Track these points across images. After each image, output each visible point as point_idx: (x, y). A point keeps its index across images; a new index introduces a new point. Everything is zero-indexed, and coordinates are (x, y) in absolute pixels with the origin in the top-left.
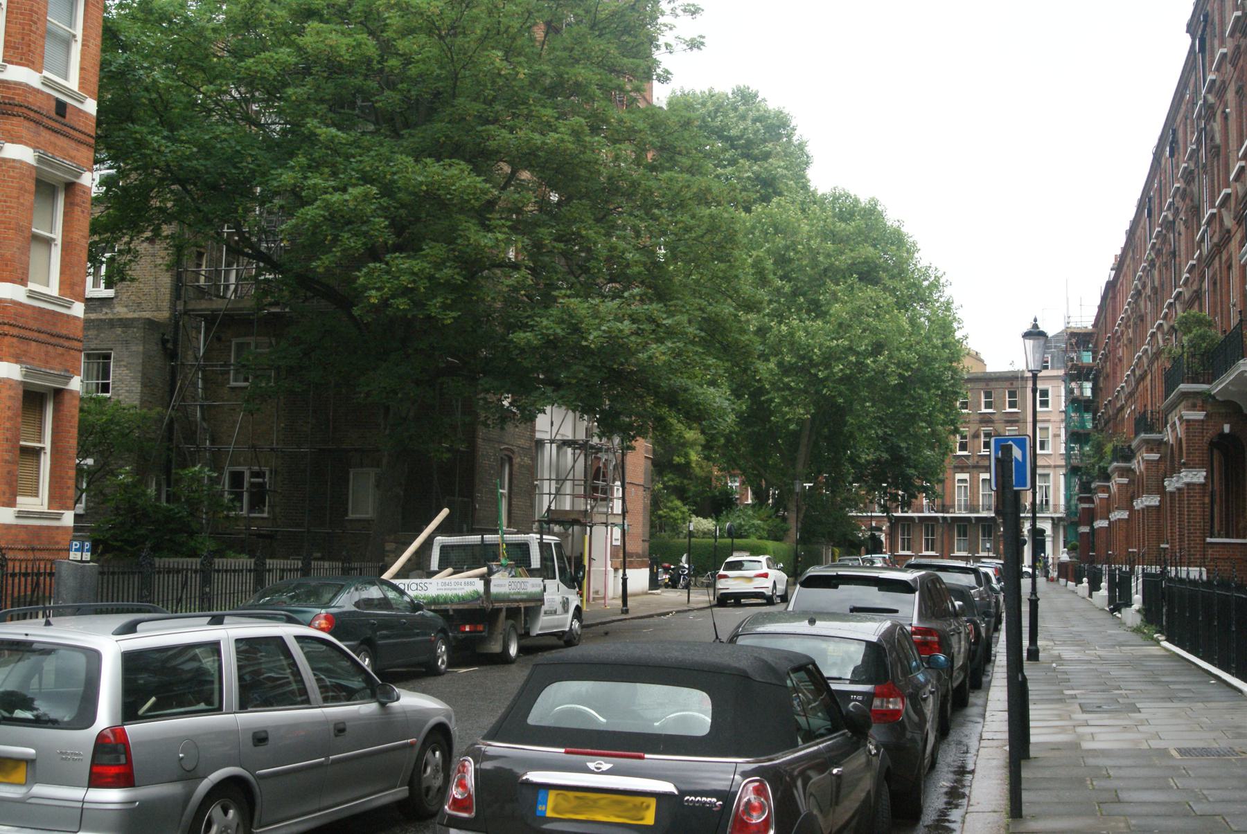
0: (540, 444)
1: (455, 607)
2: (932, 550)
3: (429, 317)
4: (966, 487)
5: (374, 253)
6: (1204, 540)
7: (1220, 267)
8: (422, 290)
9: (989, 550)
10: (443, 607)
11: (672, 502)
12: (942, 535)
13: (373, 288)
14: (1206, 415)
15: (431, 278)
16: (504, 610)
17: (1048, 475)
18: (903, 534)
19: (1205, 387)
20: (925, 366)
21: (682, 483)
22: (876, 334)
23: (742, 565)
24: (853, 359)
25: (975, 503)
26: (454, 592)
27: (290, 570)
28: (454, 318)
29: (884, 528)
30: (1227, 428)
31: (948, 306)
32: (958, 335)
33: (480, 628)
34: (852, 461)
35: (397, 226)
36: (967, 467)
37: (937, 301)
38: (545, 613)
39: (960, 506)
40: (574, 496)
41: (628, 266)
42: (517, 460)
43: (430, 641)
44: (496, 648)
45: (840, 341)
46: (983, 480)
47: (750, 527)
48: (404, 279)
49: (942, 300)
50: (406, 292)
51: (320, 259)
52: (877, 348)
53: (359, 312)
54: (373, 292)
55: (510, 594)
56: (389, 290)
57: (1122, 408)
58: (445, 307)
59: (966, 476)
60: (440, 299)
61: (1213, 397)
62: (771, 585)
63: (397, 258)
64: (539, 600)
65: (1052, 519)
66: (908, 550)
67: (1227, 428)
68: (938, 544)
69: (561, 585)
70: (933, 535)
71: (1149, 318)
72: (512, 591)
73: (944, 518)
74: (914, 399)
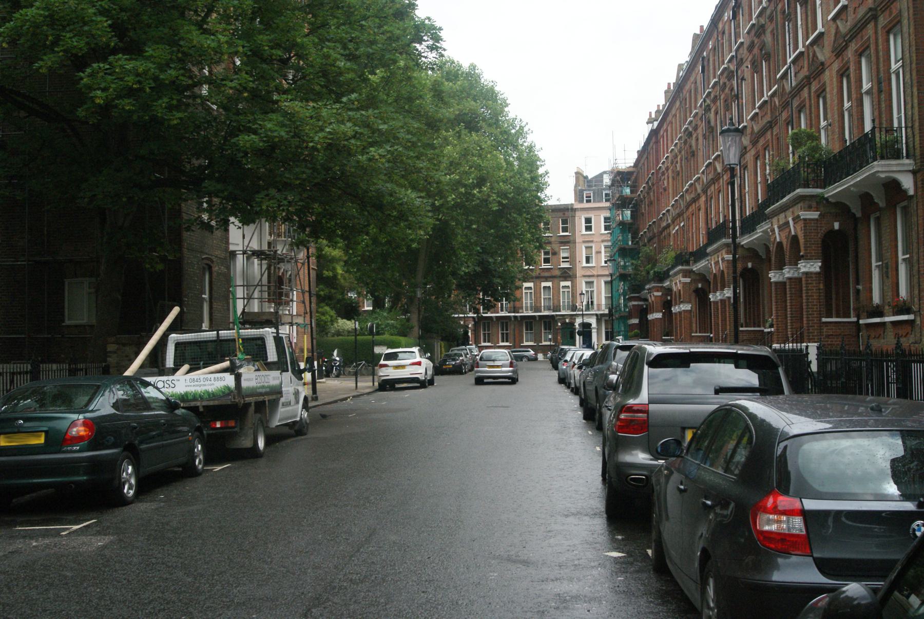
0: (233, 254)
1: (205, 403)
2: (507, 341)
3: (154, 119)
4: (531, 293)
5: (100, 53)
6: (820, 320)
7: (810, 96)
8: (148, 90)
9: (550, 340)
10: (192, 404)
11: (322, 307)
12: (514, 330)
13: (98, 89)
14: (820, 215)
15: (156, 79)
16: (253, 404)
17: (593, 282)
18: (484, 330)
19: (819, 191)
20: (519, 195)
21: (330, 292)
22: (480, 171)
23: (397, 356)
24: (463, 190)
25: (538, 305)
26: (203, 388)
27: (20, 373)
28: (181, 119)
29: (470, 326)
30: (836, 226)
31: (531, 148)
32: (541, 171)
33: (232, 423)
34: (454, 274)
35: (118, 28)
36: (532, 278)
37: (522, 145)
38: (283, 405)
39: (564, 306)
40: (261, 300)
41: (341, 74)
42: (215, 269)
43: (188, 441)
44: (247, 443)
45: (452, 176)
46: (545, 287)
47: (386, 326)
48: (130, 79)
49: (526, 144)
50: (130, 92)
51: (42, 60)
52: (481, 182)
53: (84, 113)
54: (99, 93)
55: (257, 388)
56: (115, 90)
57: (668, 226)
58: (170, 108)
59: (531, 285)
60: (166, 100)
61: (827, 199)
62: (423, 371)
63: (119, 59)
64: (277, 392)
65: (597, 315)
66: (489, 342)
67: (836, 226)
68: (511, 337)
69: (293, 377)
70: (507, 330)
71: (700, 154)
72: (259, 385)
73: (515, 317)
74: (509, 221)
